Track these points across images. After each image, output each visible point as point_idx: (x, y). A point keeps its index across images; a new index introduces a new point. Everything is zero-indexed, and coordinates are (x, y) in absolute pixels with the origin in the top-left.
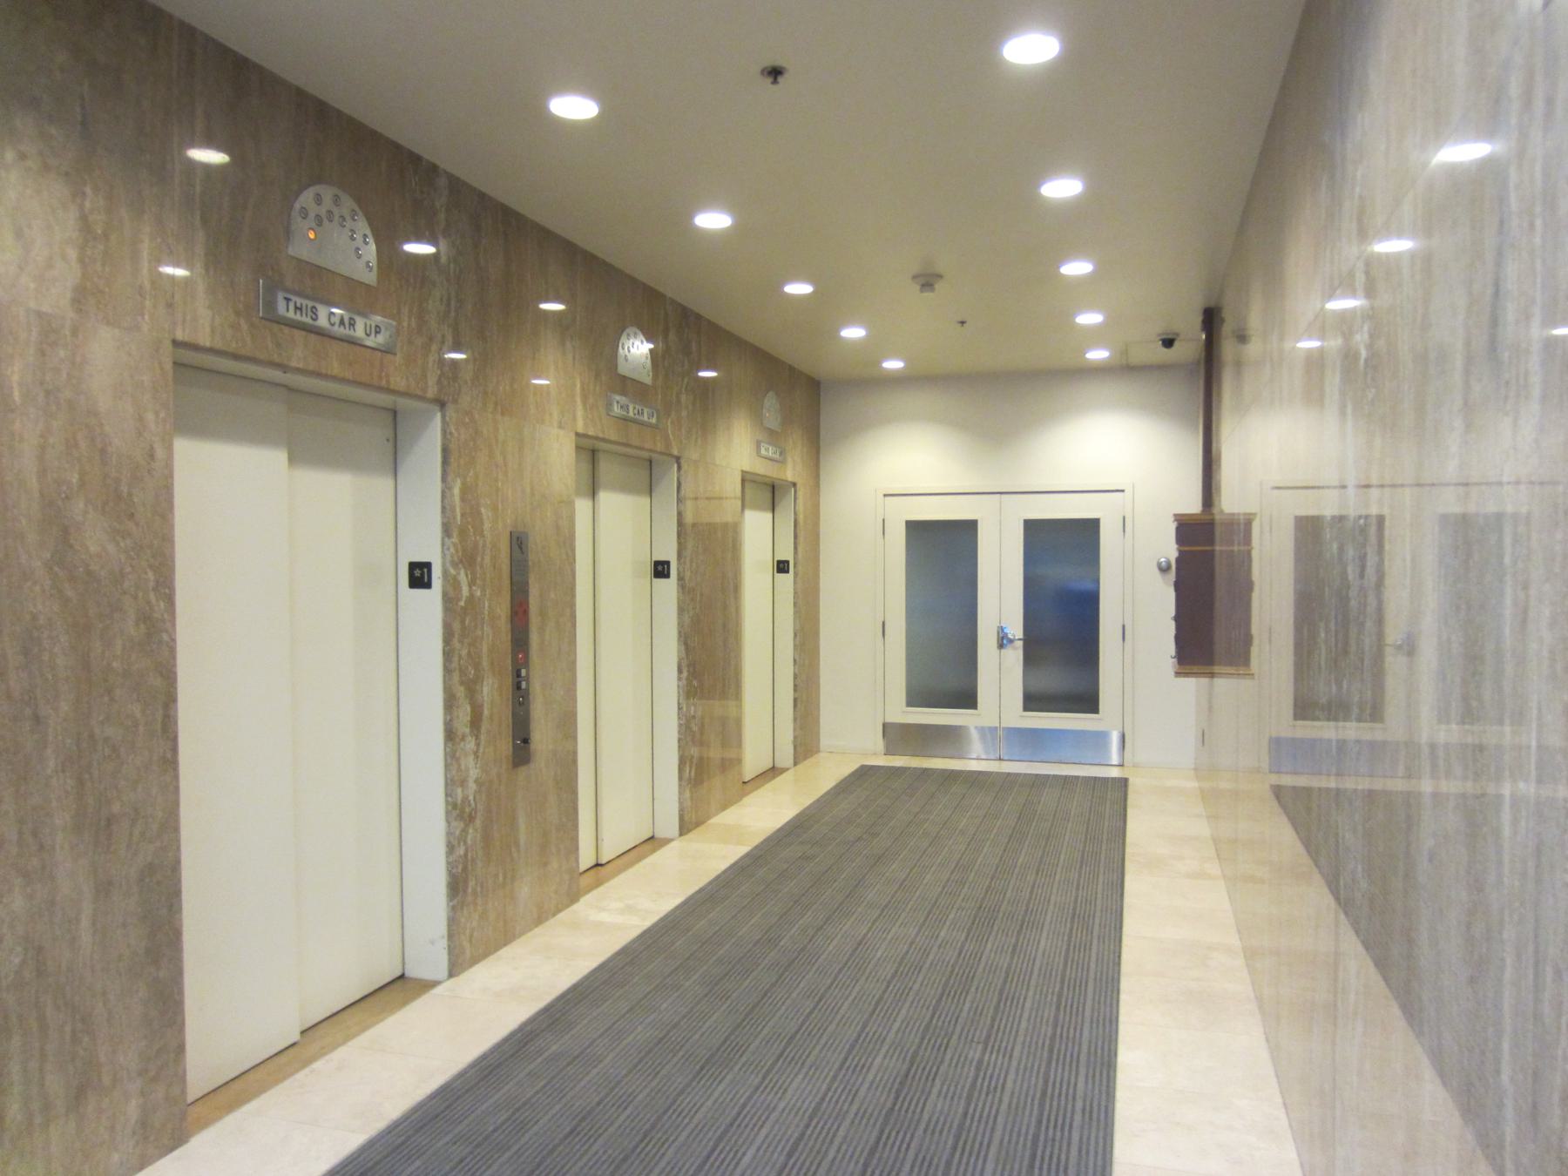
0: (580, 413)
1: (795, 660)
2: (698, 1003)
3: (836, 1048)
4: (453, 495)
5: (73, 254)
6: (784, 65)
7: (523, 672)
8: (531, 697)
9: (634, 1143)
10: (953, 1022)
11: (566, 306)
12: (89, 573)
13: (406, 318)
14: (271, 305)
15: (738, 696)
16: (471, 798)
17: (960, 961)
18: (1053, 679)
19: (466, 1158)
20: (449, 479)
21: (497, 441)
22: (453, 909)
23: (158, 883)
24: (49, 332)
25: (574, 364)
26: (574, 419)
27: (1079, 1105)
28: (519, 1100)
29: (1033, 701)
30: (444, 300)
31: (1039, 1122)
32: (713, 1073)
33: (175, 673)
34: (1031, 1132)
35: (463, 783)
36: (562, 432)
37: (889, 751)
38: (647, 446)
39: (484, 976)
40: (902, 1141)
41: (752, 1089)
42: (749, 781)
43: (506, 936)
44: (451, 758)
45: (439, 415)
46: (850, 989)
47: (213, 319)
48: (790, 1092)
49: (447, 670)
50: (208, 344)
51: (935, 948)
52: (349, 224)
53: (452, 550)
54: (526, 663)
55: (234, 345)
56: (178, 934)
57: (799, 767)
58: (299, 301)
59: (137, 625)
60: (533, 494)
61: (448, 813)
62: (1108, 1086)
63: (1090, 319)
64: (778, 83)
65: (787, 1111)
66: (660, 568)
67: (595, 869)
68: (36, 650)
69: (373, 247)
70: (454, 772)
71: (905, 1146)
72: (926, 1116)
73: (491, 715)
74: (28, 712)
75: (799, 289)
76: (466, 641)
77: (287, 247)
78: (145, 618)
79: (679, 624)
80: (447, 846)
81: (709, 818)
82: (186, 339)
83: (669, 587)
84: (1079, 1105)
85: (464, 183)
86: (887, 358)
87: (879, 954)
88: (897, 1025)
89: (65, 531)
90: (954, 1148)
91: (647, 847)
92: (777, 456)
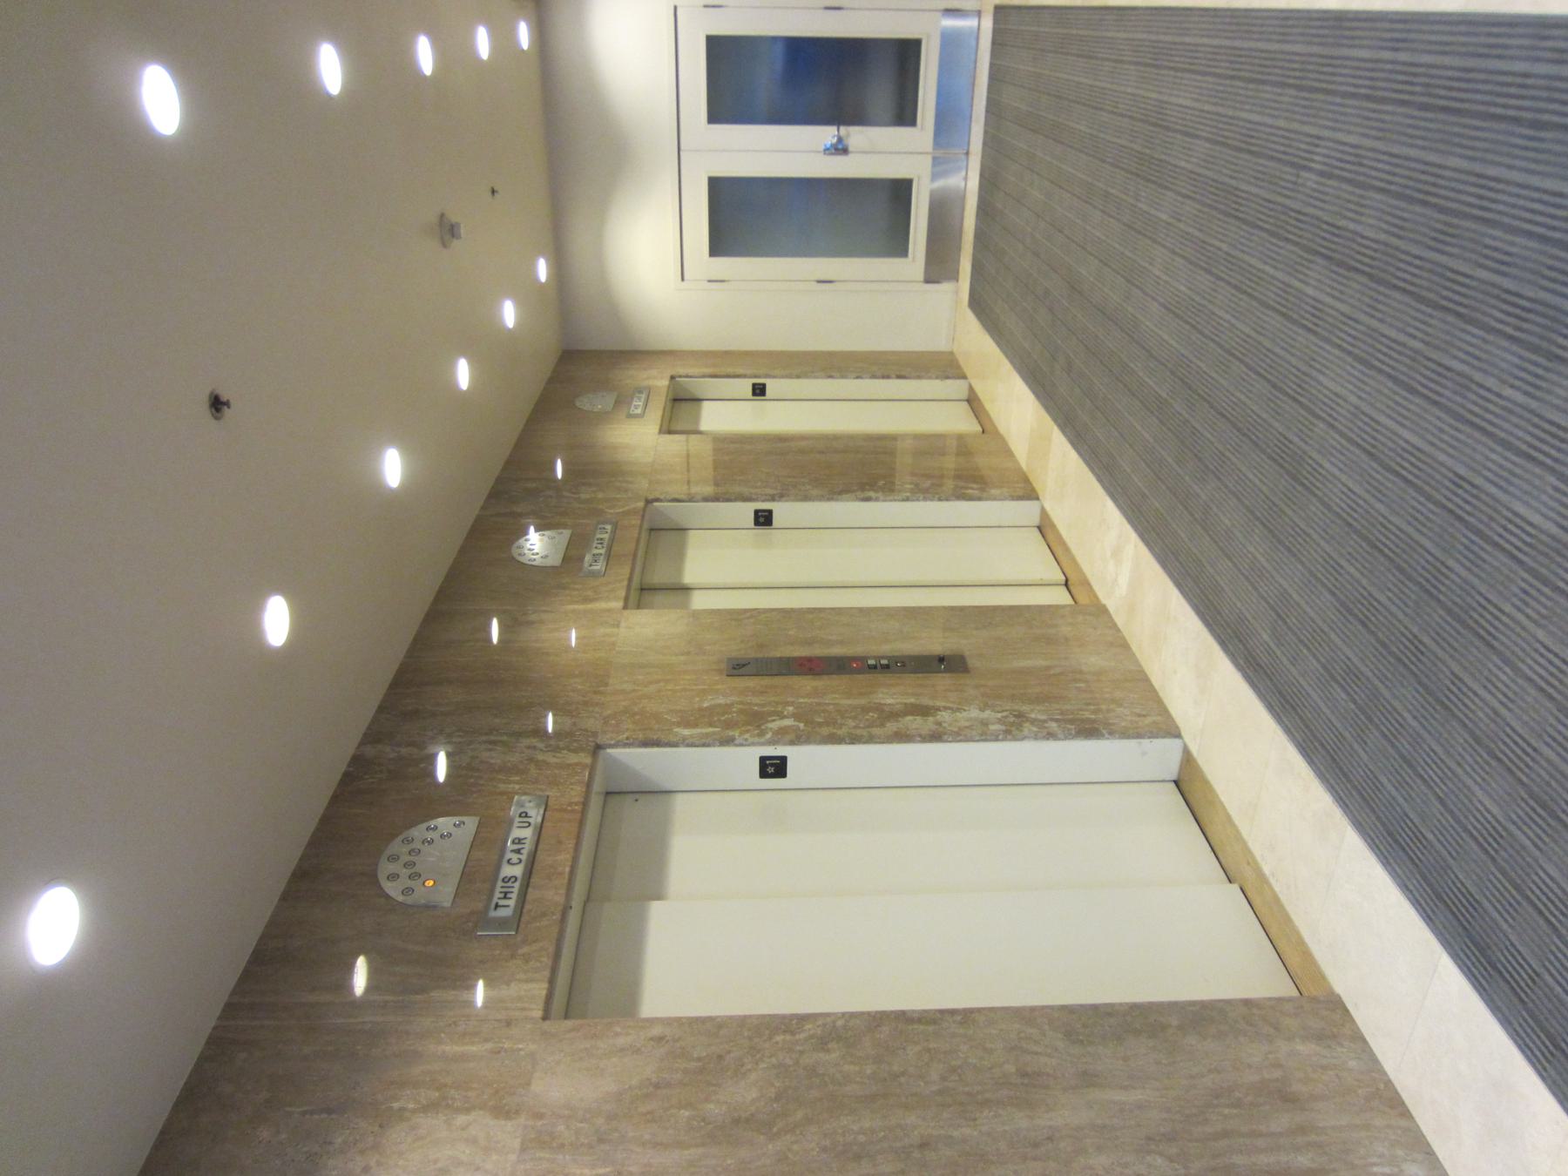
0: (603, 605)
1: (857, 378)
2: (1226, 487)
3: (1289, 337)
4: (691, 736)
5: (461, 1119)
6: (207, 392)
7: (871, 662)
8: (896, 654)
9: (1382, 559)
10: (1271, 206)
11: (493, 617)
12: (778, 1098)
13: (511, 786)
14: (502, 923)
15: (893, 438)
16: (999, 715)
17: (1198, 197)
18: (880, 93)
19: (1382, 732)
20: (673, 739)
21: (634, 690)
22: (1111, 733)
23: (1085, 1026)
24: (541, 1140)
25: (552, 612)
26: (609, 610)
27: (1387, 55)
28: (1322, 675)
29: (905, 115)
30: (490, 747)
31: (1403, 103)
32: (1308, 472)
33: (877, 1012)
34: (1416, 113)
35: (985, 723)
36: (623, 624)
37: (953, 276)
38: (635, 534)
39: (1181, 701)
40: (1409, 264)
41: (1332, 432)
42: (981, 426)
43: (1140, 680)
44: (960, 735)
45: (609, 751)
46: (1221, 322)
47: (520, 981)
48: (1339, 390)
49: (871, 740)
50: (546, 985)
51: (1182, 226)
52: (417, 845)
53: (747, 736)
54: (861, 659)
55: (545, 959)
56: (1134, 1007)
57: (968, 375)
58: (497, 895)
59: (828, 1051)
60: (688, 653)
61: (1015, 739)
62: (1365, 20)
63: (483, 43)
64: (228, 401)
65: (1360, 393)
67: (1071, 588)
68: (855, 1148)
69: (441, 820)
70: (974, 733)
71: (1417, 262)
72: (1383, 237)
73: (914, 695)
74: (916, 1154)
75: (463, 374)
76: (839, 721)
77: (443, 908)
78: (822, 1043)
79: (820, 500)
80: (1048, 739)
81: (1020, 469)
82: (541, 1006)
83: (781, 511)
84: (1387, 55)
85: (369, 728)
86: (537, 279)
87: (1183, 288)
88: (1267, 268)
89: (736, 1121)
90: (1425, 203)
91: (1050, 537)
92: (643, 396)
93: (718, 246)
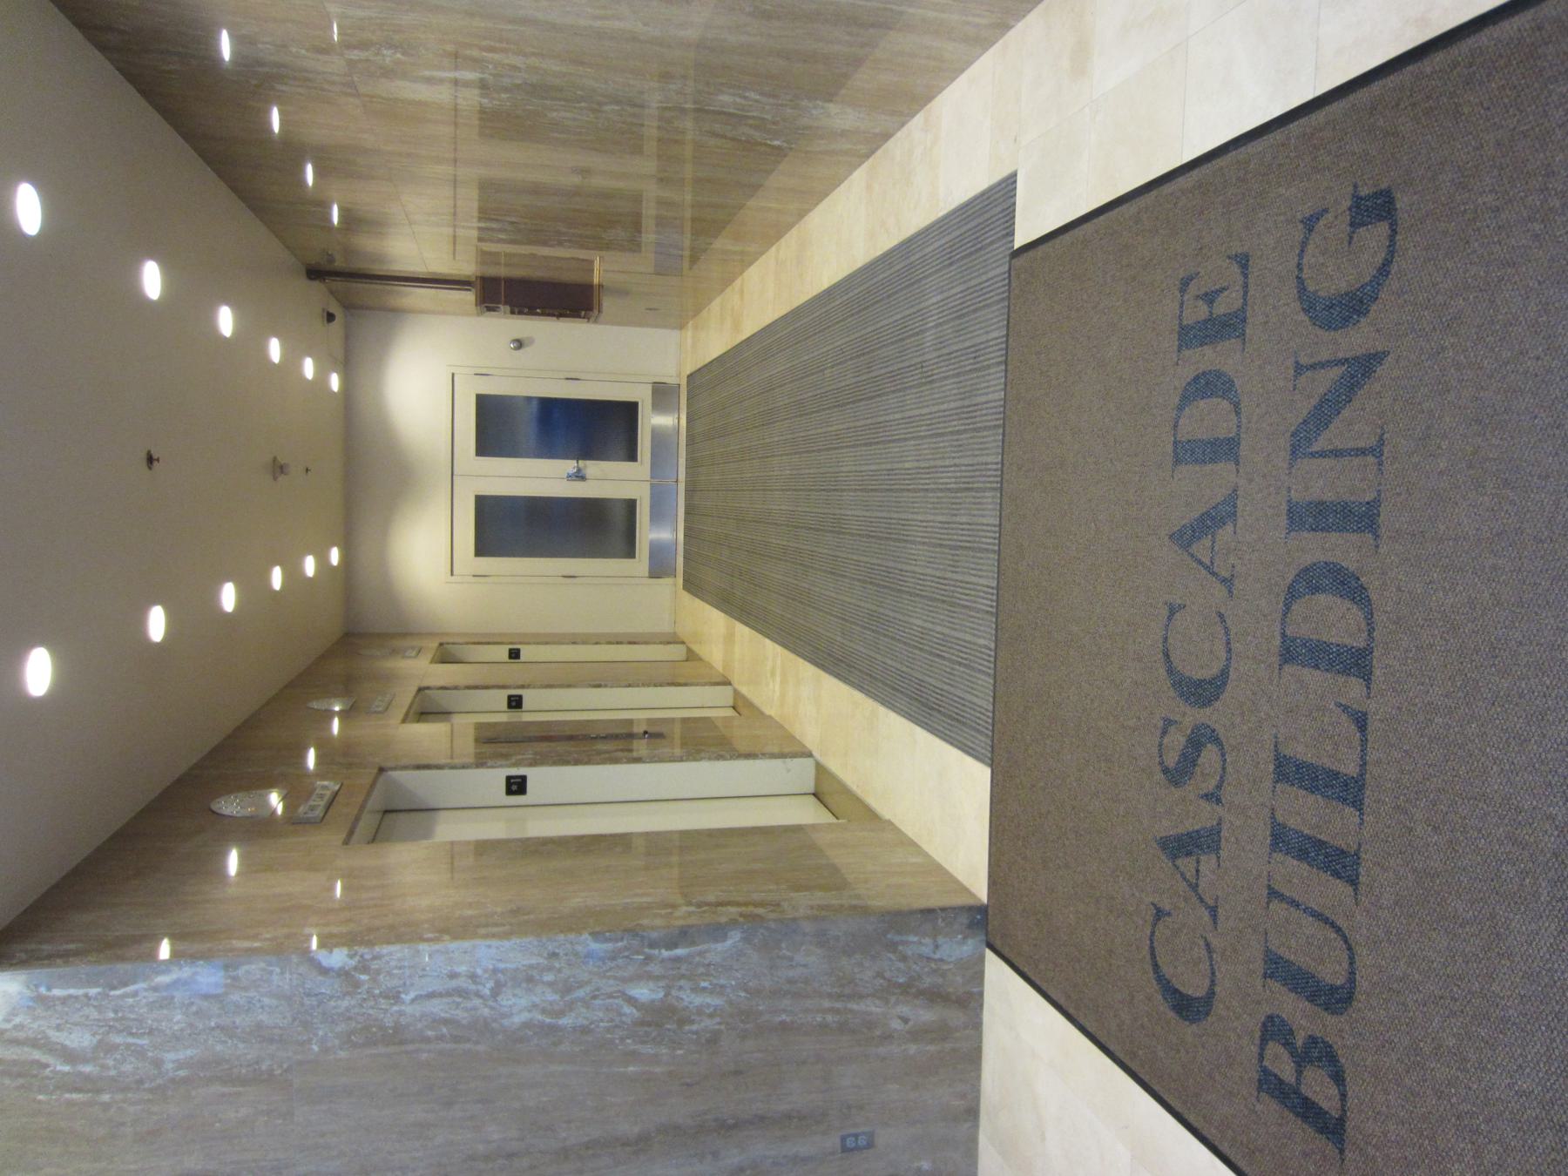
45: (390, 773)
66: (514, 704)
93: (482, 549)
